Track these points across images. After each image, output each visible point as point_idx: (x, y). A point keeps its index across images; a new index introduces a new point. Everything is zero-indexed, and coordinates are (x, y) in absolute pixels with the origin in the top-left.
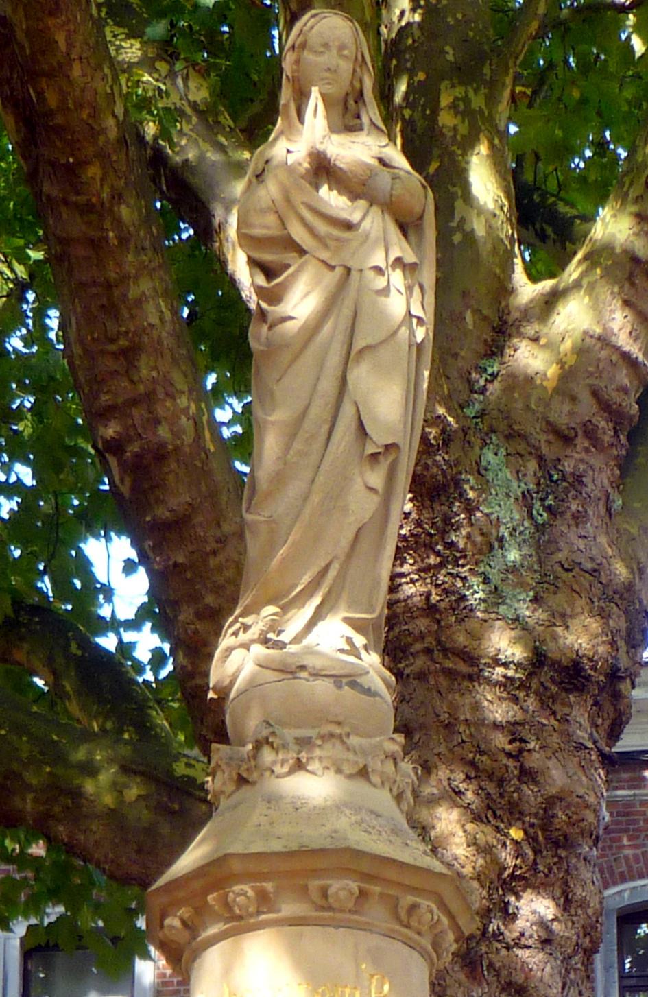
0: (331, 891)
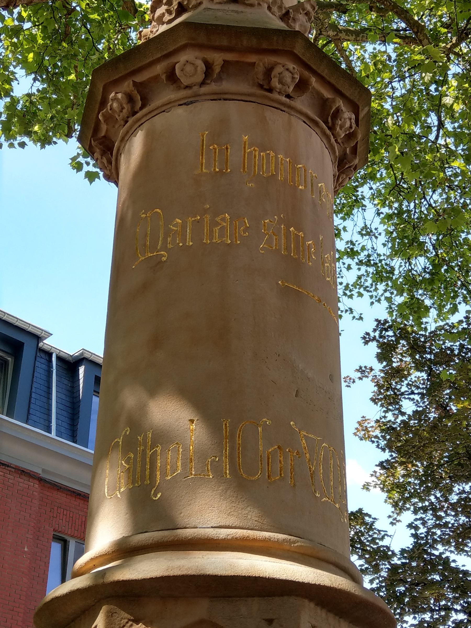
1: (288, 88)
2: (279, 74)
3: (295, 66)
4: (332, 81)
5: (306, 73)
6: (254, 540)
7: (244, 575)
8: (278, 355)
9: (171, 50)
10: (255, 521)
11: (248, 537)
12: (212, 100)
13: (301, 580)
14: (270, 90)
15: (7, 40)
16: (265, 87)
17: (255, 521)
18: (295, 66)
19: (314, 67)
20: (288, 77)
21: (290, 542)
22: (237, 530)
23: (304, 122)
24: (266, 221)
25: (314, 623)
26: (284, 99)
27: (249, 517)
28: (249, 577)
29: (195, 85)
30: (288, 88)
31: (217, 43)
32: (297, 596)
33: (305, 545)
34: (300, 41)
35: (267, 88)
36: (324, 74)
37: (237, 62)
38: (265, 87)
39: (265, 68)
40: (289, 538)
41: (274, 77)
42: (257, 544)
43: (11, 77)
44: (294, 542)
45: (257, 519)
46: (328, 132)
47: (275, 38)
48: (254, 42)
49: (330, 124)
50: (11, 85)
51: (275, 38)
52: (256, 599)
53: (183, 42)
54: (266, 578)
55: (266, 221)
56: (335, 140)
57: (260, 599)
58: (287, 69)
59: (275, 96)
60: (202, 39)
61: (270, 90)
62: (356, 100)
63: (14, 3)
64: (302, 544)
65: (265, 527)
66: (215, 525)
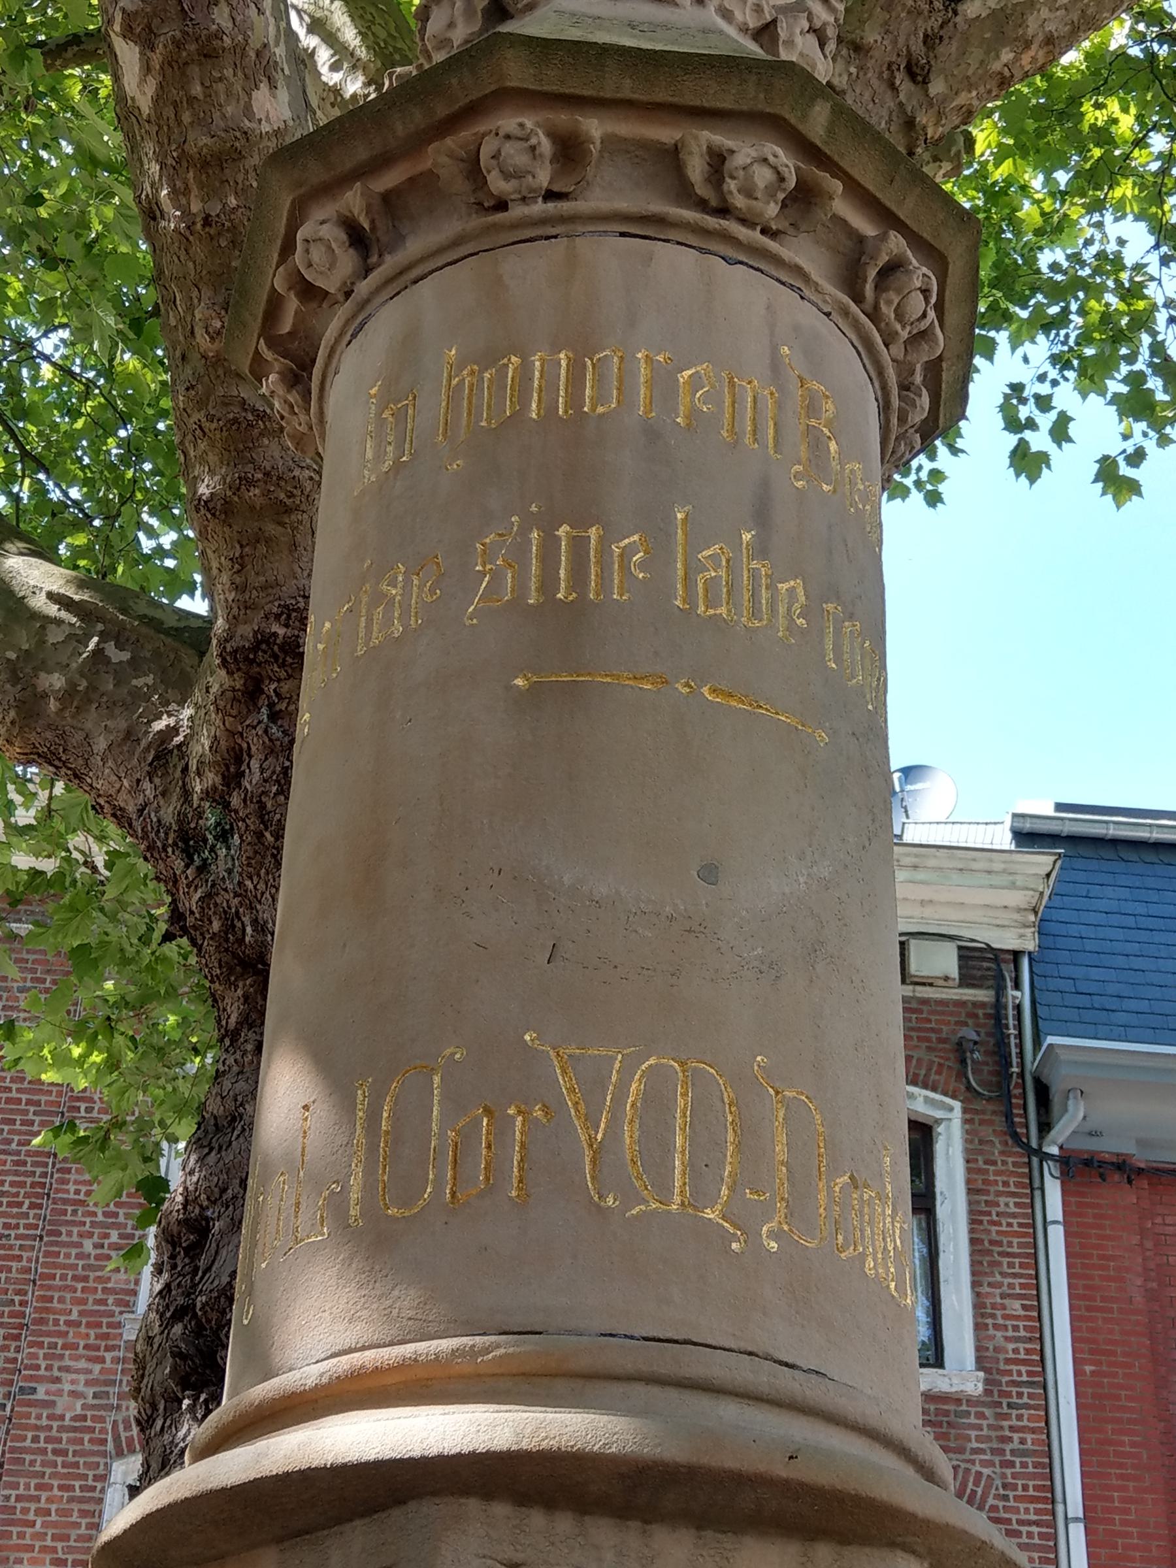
0: (740, 160)
1: (534, 177)
2: (493, 157)
3: (520, 120)
4: (661, 96)
5: (562, 118)
6: (377, 1371)
7: (274, 1473)
8: (496, 872)
9: (282, 230)
10: (410, 1319)
11: (362, 1367)
12: (391, 298)
13: (417, 1453)
14: (502, 205)
15: (1076, 204)
16: (486, 204)
17: (410, 1319)
18: (520, 120)
19: (587, 92)
20: (515, 155)
21: (473, 1352)
22: (352, 1355)
23: (623, 234)
24: (488, 541)
25: (510, 1554)
26: (539, 208)
27: (395, 1312)
28: (287, 1474)
29: (353, 283)
30: (534, 177)
31: (349, 165)
32: (434, 1494)
33: (518, 1350)
34: (509, 54)
35: (492, 203)
36: (626, 93)
37: (412, 180)
38: (486, 204)
39: (462, 160)
40: (471, 1343)
41: (489, 172)
42: (389, 1380)
43: (1138, 279)
44: (487, 1350)
45: (411, 1313)
46: (712, 222)
47: (454, 81)
48: (418, 118)
49: (714, 203)
50: (1145, 297)
51: (454, 81)
52: (358, 1523)
53: (286, 203)
54: (325, 1468)
55: (488, 541)
56: (763, 232)
57: (367, 1520)
58: (508, 137)
59: (517, 211)
60: (316, 173)
61: (502, 205)
62: (761, 106)
63: (922, 138)
64: (511, 1350)
65: (432, 1330)
66: (323, 1356)
